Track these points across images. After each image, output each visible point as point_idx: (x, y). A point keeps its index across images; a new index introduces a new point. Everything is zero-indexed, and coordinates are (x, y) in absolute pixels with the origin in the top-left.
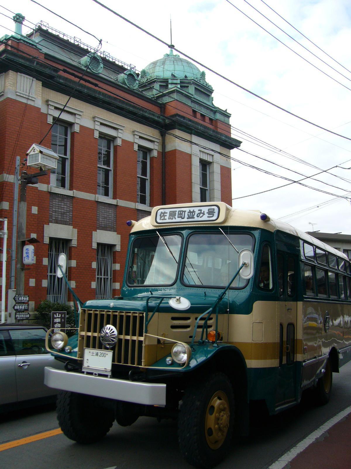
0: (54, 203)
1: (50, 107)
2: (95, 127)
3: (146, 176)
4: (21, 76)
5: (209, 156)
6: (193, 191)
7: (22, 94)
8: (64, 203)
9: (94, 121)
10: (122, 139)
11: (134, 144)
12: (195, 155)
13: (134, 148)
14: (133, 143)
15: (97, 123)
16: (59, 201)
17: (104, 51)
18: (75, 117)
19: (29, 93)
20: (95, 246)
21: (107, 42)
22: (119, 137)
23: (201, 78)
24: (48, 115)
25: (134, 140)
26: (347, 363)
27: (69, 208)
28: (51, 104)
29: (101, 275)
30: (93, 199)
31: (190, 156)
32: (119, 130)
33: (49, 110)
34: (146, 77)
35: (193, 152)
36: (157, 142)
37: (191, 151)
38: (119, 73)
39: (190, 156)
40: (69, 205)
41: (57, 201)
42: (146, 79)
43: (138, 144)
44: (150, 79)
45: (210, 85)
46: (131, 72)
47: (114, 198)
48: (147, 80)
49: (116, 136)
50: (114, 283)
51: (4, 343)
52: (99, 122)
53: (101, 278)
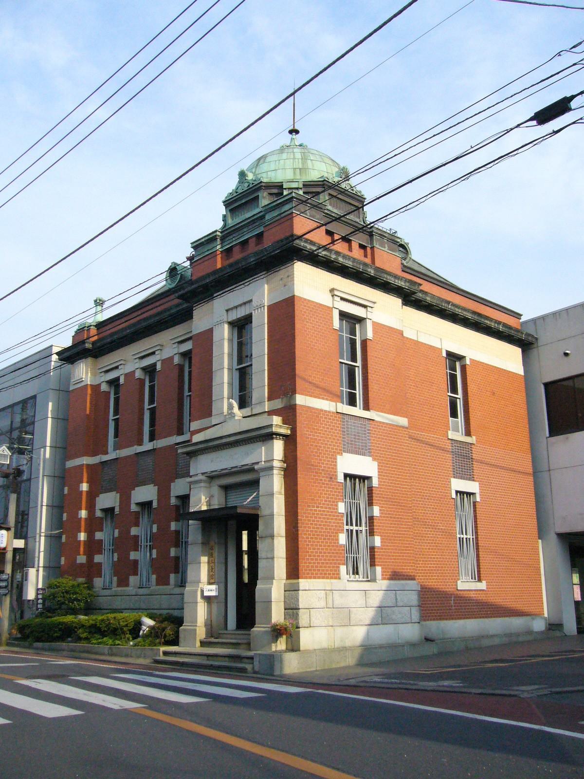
2: (333, 305)
3: (356, 362)
9: (333, 296)
11: (332, 311)
14: (332, 308)
15: (336, 298)
20: (341, 478)
24: (333, 308)
25: (333, 303)
29: (352, 525)
30: (333, 410)
33: (335, 302)
34: (246, 181)
38: (333, 205)
42: (246, 185)
43: (339, 310)
44: (253, 184)
47: (366, 407)
48: (249, 186)
50: (178, 529)
51: (271, 586)
53: (352, 531)
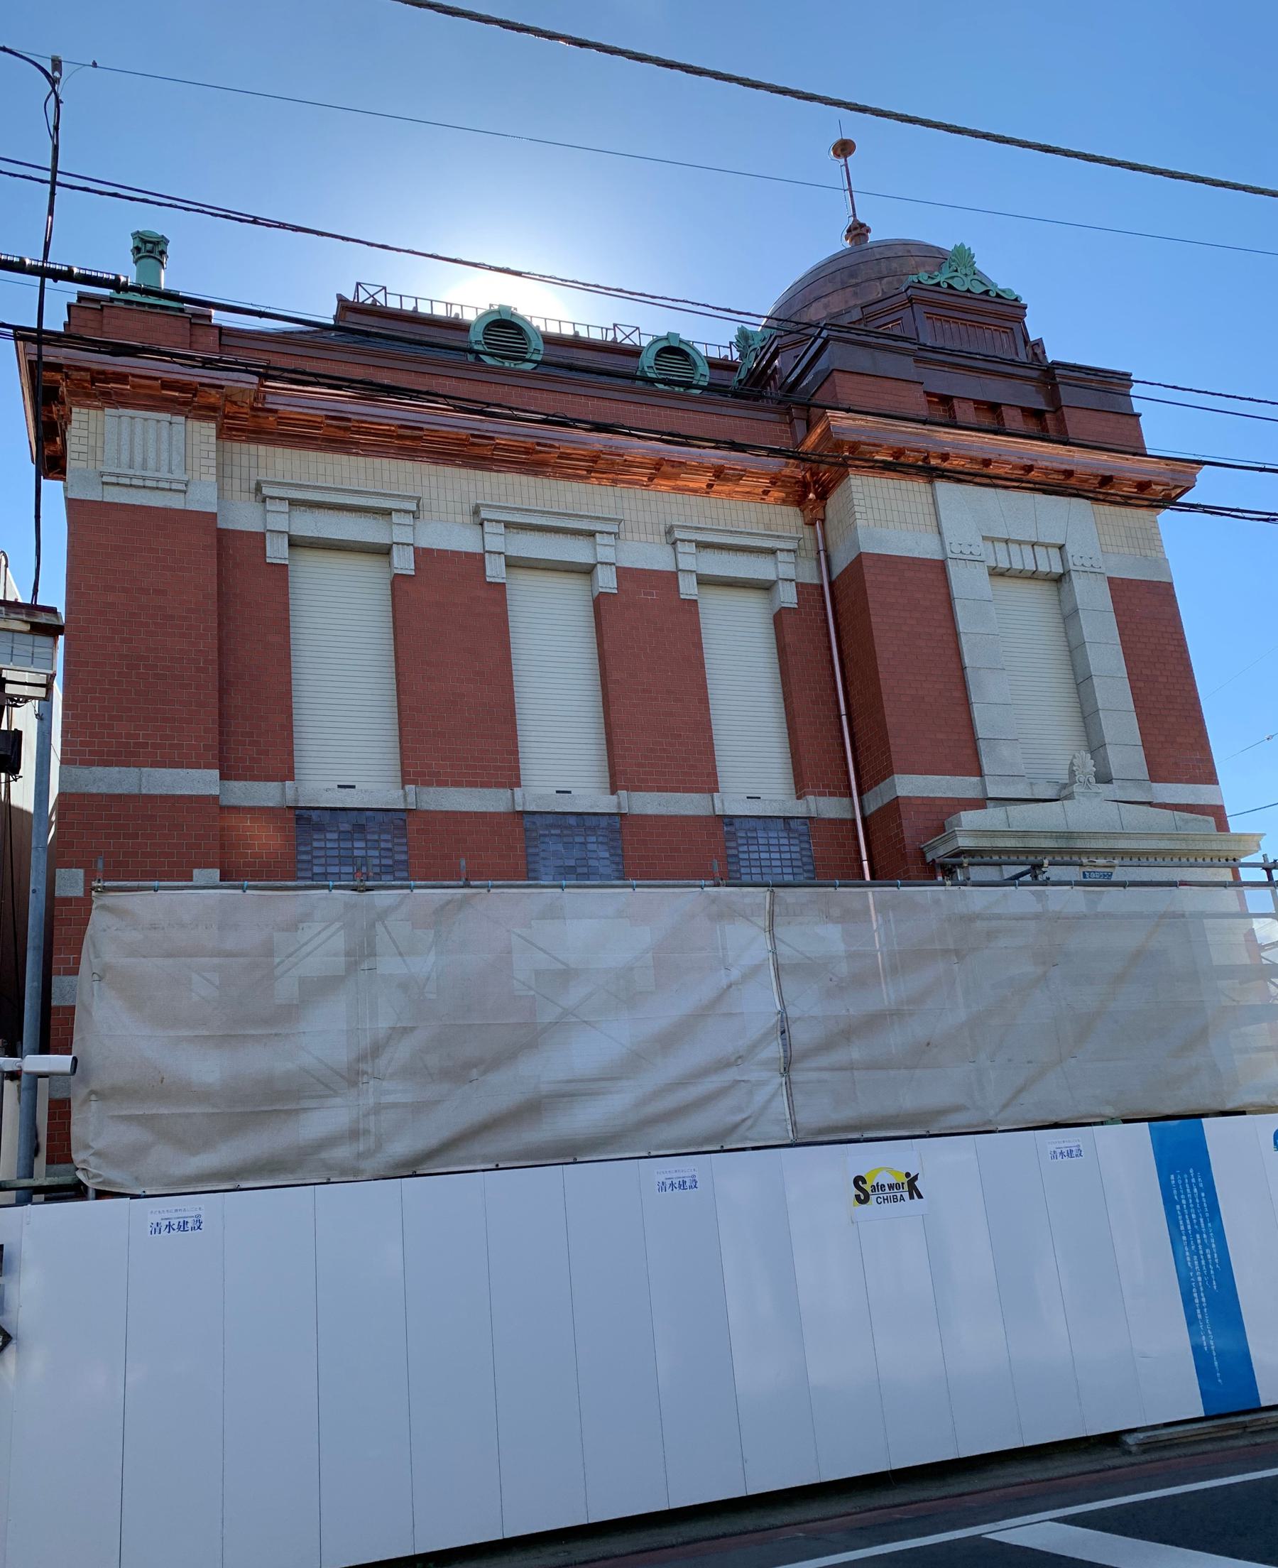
0: (315, 844)
1: (270, 505)
4: (120, 417)
5: (1014, 548)
6: (973, 700)
7: (126, 476)
8: (366, 841)
10: (617, 568)
11: (677, 575)
12: (965, 557)
13: (678, 591)
16: (382, 852)
17: (615, 325)
18: (391, 523)
19: (170, 471)
21: (95, 65)
22: (602, 563)
23: (955, 274)
26: (450, 809)
27: (390, 854)
28: (270, 494)
31: (940, 568)
32: (597, 534)
34: (751, 348)
35: (948, 548)
36: (789, 551)
37: (943, 548)
39: (940, 568)
40: (389, 845)
41: (335, 836)
45: (1003, 291)
46: (669, 342)
49: (592, 561)
52: (498, 521)
